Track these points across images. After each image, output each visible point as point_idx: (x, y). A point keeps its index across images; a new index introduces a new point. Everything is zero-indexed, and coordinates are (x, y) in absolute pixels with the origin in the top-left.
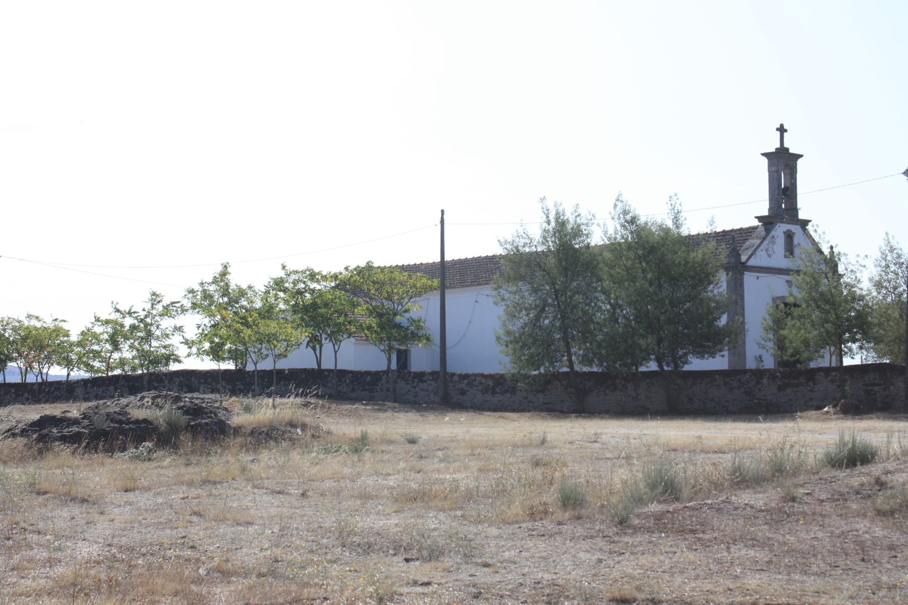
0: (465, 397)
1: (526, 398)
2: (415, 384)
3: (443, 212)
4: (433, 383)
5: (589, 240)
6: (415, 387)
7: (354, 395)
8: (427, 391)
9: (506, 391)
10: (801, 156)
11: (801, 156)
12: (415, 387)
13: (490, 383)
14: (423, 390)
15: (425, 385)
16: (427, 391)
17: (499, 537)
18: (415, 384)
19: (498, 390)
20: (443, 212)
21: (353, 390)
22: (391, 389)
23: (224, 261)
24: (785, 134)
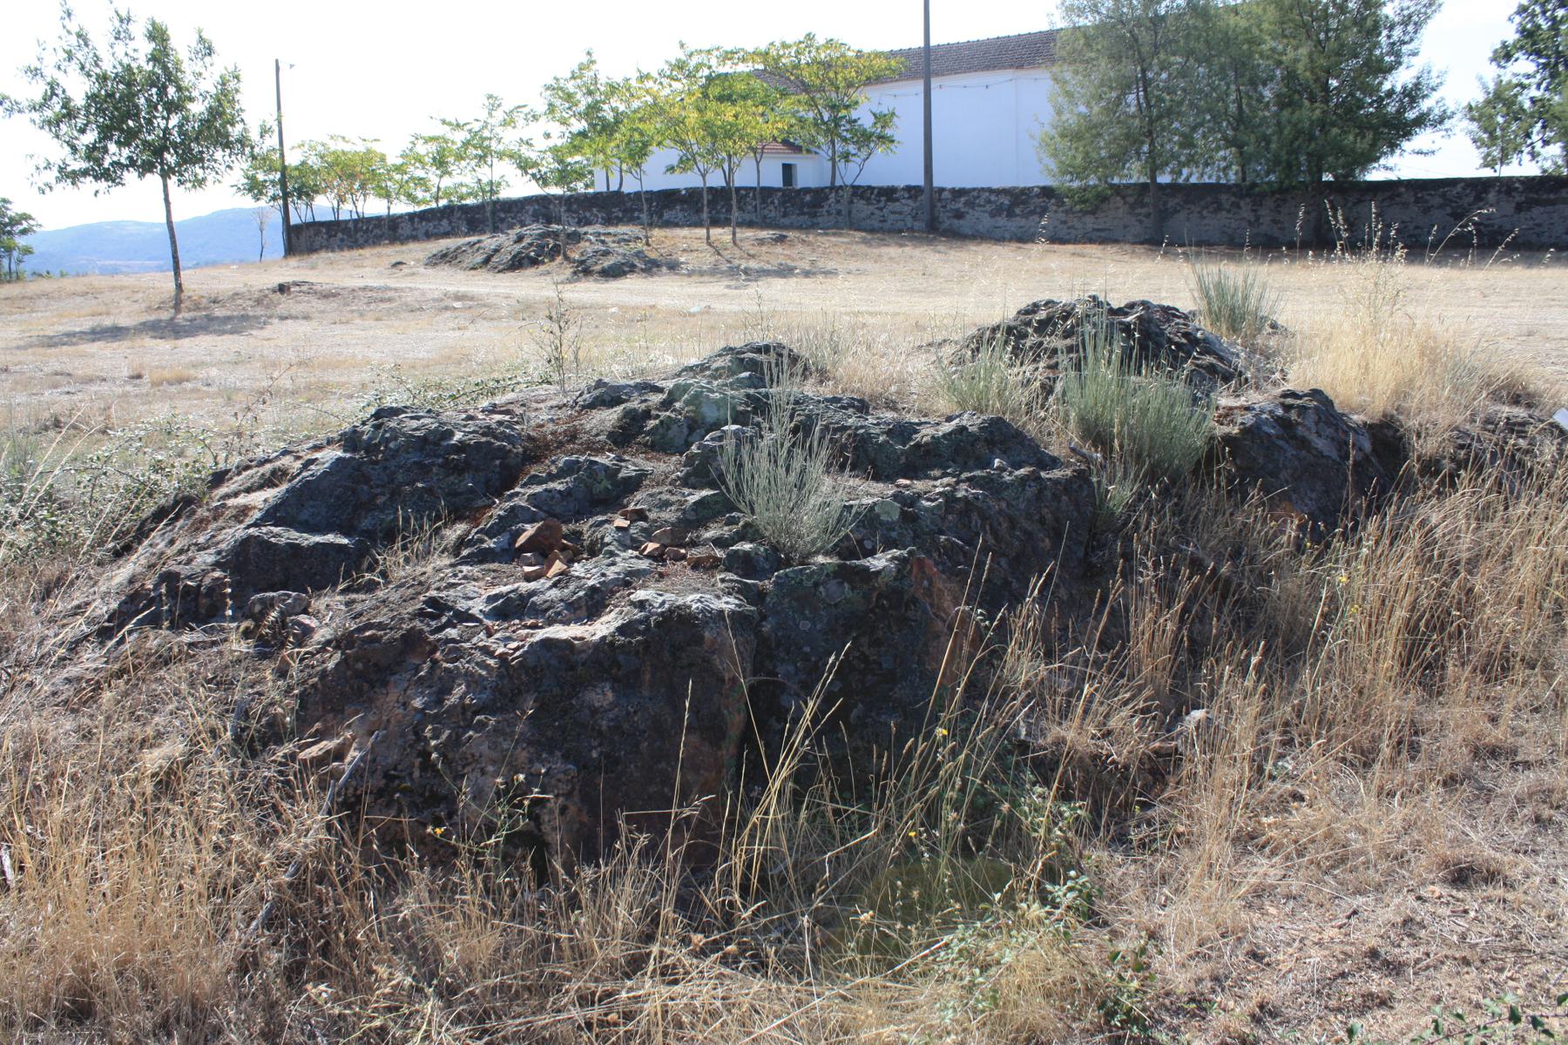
1: (1065, 222)
7: (786, 221)
15: (897, 206)
19: (1017, 211)
21: (785, 215)
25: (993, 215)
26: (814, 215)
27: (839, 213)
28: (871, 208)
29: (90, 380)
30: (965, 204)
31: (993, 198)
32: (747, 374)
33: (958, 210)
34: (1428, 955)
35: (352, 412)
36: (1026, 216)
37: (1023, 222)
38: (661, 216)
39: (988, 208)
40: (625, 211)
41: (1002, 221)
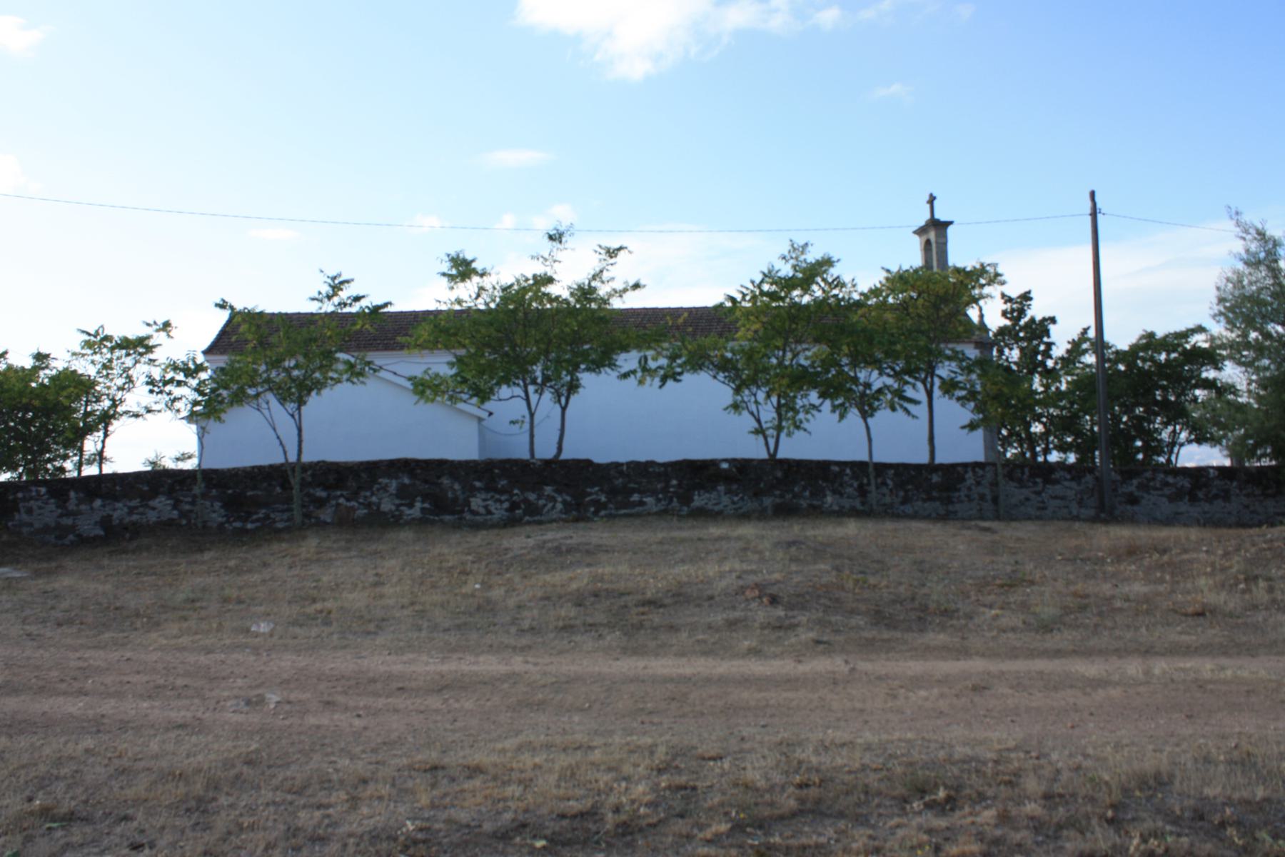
0: (1136, 508)
1: (1247, 507)
2: (1039, 488)
3: (1093, 194)
4: (1073, 484)
5: (200, 359)
6: (1038, 493)
7: (908, 509)
8: (1063, 498)
9: (1216, 497)
10: (951, 223)
11: (951, 223)
12: (1038, 493)
13: (1186, 483)
14: (1056, 497)
15: (1057, 490)
16: (1063, 498)
17: (264, 581)
18: (1039, 488)
19: (1200, 495)
20: (1093, 194)
21: (905, 501)
22: (989, 497)
23: (642, 282)
24: (936, 202)
25: (1172, 499)
26: (949, 501)
27: (982, 497)
28: (1026, 492)
29: (622, 594)
30: (1140, 487)
31: (1170, 480)
32: (146, 488)
33: (1131, 494)
34: (643, 723)
35: (1212, 296)
36: (1210, 500)
37: (1207, 507)
38: (686, 500)
39: (1167, 491)
40: (612, 492)
41: (1184, 506)
